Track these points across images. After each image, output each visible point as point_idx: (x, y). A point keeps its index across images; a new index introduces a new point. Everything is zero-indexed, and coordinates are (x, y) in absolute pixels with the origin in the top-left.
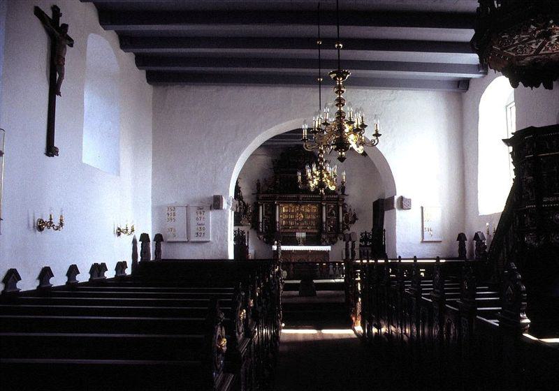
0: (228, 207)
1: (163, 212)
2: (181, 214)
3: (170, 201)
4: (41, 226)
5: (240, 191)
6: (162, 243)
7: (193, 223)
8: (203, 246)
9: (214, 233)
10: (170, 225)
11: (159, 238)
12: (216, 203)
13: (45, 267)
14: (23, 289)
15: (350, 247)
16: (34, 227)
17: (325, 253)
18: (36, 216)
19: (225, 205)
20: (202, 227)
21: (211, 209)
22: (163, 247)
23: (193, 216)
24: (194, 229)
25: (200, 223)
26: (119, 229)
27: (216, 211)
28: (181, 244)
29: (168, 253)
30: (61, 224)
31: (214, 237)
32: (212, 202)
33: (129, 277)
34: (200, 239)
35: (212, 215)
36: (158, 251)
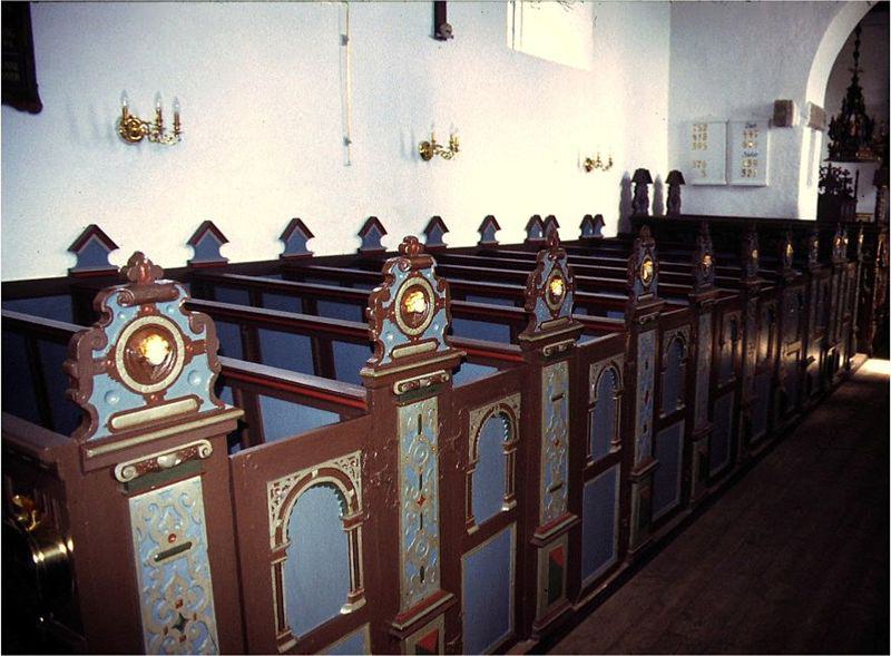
0: (802, 123)
1: (690, 133)
2: (716, 136)
3: (698, 114)
4: (427, 152)
5: (860, 96)
6: (681, 186)
7: (738, 150)
8: (754, 193)
9: (775, 170)
10: (696, 155)
11: (676, 179)
12: (781, 115)
13: (435, 217)
14: (318, 253)
15: (665, 196)
16: (413, 154)
17: (624, 283)
18: (416, 135)
19: (797, 119)
20: (752, 159)
21: (770, 126)
22: (684, 194)
23: (738, 141)
24: (738, 163)
25: (750, 151)
26: (588, 160)
27: (782, 131)
28: (715, 190)
29: (691, 204)
30: (611, 164)
31: (772, 178)
32: (771, 114)
33: (610, 241)
34: (750, 182)
35: (771, 138)
36: (674, 199)
